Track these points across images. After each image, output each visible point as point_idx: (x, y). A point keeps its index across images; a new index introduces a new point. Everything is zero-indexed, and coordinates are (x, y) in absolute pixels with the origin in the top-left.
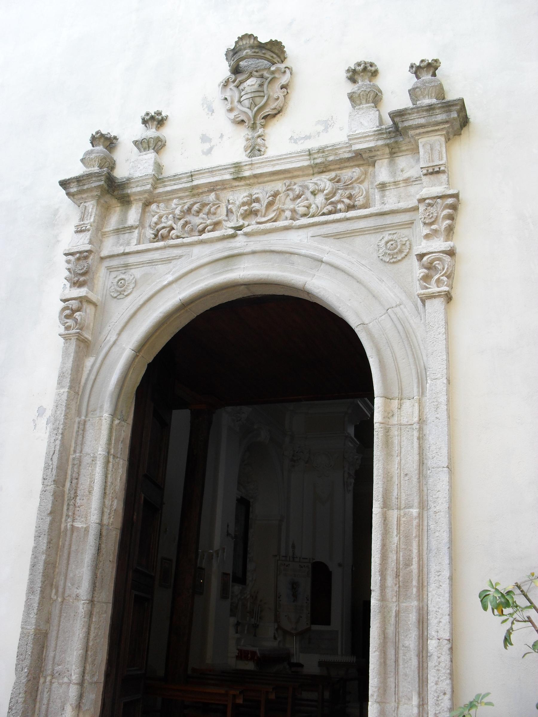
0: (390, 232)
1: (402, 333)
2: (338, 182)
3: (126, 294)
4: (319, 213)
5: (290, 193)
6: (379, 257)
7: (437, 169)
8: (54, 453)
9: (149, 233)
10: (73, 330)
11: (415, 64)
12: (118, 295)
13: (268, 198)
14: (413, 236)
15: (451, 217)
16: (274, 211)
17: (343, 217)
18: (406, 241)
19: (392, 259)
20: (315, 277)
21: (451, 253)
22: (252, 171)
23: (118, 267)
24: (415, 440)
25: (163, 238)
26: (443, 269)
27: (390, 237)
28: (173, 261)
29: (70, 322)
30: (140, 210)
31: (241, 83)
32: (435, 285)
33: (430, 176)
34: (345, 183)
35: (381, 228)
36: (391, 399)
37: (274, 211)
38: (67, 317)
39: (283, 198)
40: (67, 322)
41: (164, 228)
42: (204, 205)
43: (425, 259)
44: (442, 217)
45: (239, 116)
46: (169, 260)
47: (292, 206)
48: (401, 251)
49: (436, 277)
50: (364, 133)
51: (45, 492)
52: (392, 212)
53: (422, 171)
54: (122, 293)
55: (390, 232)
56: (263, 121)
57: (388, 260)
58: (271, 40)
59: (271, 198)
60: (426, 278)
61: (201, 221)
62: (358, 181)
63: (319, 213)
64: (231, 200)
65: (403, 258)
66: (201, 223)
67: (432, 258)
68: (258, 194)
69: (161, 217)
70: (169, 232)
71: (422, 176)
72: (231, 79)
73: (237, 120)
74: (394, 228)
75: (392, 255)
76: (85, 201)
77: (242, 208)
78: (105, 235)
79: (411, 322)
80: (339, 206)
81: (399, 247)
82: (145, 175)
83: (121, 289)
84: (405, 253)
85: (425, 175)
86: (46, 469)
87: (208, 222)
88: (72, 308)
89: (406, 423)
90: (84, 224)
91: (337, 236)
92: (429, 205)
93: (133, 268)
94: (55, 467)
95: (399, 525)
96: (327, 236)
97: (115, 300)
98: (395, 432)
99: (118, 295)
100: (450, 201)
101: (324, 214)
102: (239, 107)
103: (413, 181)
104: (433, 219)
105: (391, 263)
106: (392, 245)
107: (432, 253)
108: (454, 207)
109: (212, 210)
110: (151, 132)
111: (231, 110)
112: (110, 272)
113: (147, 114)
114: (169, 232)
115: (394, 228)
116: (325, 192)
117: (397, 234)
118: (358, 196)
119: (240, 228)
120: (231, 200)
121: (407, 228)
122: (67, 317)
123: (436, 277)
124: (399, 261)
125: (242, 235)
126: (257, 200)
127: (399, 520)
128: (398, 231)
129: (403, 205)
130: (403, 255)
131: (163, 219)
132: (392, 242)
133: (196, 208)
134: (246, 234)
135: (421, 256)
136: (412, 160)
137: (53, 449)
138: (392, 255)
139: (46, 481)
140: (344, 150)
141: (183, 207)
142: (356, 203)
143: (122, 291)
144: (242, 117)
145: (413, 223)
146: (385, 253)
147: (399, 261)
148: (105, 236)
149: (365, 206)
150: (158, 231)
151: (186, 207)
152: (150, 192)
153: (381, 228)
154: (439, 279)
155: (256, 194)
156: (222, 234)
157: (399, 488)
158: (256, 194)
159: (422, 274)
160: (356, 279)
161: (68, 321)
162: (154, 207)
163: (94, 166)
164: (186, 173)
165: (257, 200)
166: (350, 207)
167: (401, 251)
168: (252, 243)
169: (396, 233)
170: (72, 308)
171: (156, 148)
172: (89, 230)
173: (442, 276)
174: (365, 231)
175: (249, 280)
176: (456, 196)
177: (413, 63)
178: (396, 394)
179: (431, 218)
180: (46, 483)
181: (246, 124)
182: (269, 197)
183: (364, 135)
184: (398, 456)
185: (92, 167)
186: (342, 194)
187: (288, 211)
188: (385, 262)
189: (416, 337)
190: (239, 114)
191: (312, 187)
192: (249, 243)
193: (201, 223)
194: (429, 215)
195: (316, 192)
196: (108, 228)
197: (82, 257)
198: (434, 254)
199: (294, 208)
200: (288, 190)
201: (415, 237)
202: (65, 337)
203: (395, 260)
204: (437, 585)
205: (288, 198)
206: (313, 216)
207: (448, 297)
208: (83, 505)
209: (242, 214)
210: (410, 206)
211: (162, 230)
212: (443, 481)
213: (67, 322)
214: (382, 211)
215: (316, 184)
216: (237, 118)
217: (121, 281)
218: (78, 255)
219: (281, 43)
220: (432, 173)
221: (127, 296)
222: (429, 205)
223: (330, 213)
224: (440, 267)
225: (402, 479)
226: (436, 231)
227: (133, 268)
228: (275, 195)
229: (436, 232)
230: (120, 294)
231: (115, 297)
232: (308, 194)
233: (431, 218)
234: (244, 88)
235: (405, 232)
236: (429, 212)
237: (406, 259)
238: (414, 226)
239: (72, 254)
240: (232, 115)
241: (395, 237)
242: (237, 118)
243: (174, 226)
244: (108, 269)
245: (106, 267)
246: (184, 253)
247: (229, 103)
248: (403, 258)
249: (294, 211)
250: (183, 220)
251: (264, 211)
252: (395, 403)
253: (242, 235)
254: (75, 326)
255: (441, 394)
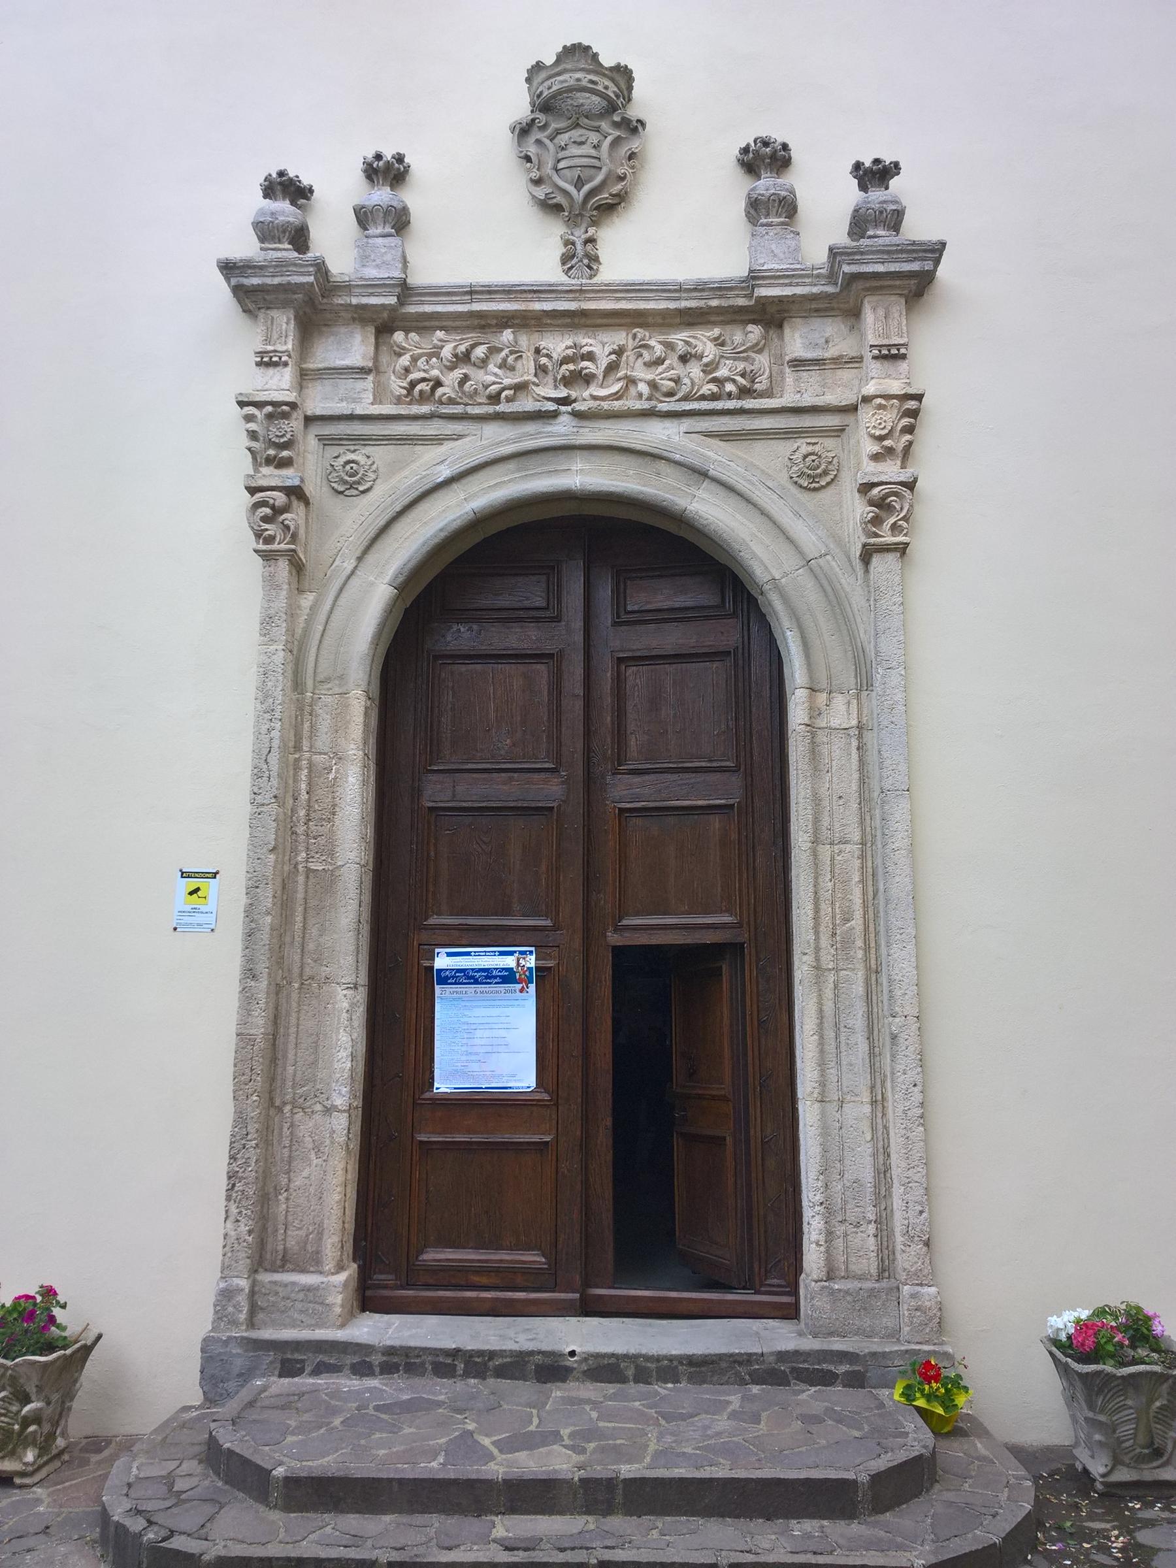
0: (809, 440)
1: (832, 597)
2: (722, 344)
3: (361, 488)
4: (695, 394)
5: (645, 353)
6: (792, 478)
7: (894, 351)
8: (270, 751)
9: (397, 386)
10: (279, 544)
11: (863, 164)
12: (347, 489)
13: (607, 356)
14: (843, 452)
15: (909, 430)
16: (619, 379)
17: (738, 406)
18: (833, 457)
19: (811, 483)
20: (696, 499)
21: (910, 485)
22: (580, 303)
23: (340, 439)
24: (854, 751)
25: (423, 398)
26: (902, 509)
27: (810, 449)
28: (446, 443)
29: (271, 529)
30: (373, 340)
31: (558, 133)
32: (889, 533)
33: (883, 360)
34: (734, 348)
35: (796, 433)
36: (816, 691)
37: (619, 379)
38: (265, 519)
39: (632, 359)
40: (267, 530)
41: (424, 380)
42: (494, 350)
43: (876, 491)
44: (899, 429)
45: (553, 195)
46: (438, 440)
47: (650, 377)
48: (825, 473)
49: (892, 520)
50: (778, 270)
51: (259, 814)
52: (814, 410)
53: (871, 351)
54: (355, 486)
55: (809, 440)
56: (595, 213)
57: (806, 485)
58: (619, 64)
59: (613, 357)
60: (877, 521)
61: (493, 379)
62: (756, 349)
63: (695, 394)
64: (544, 348)
65: (828, 484)
66: (494, 383)
67: (887, 491)
68: (591, 345)
69: (415, 359)
70: (433, 389)
71: (868, 356)
72: (539, 122)
73: (550, 202)
74: (813, 435)
75: (813, 478)
76: (268, 306)
77: (564, 367)
78: (306, 375)
79: (843, 581)
80: (729, 387)
81: (823, 467)
82: (389, 278)
83: (352, 479)
84: (832, 477)
85: (875, 358)
86: (256, 777)
87: (507, 381)
88: (274, 504)
89: (838, 727)
90: (275, 351)
91: (726, 436)
92: (880, 407)
93: (370, 445)
94: (274, 774)
95: (833, 865)
96: (709, 435)
97: (341, 497)
98: (822, 737)
99: (347, 489)
100: (912, 404)
101: (703, 398)
102: (556, 178)
103: (845, 362)
104: (886, 431)
105: (810, 489)
106: (813, 461)
107: (887, 483)
108: (914, 414)
109: (510, 360)
110: (382, 195)
111: (537, 182)
112: (325, 445)
113: (379, 157)
114: (433, 389)
115: (813, 435)
116: (705, 360)
117: (819, 445)
118: (757, 375)
119: (565, 401)
120: (544, 348)
121: (832, 436)
122: (265, 519)
123: (892, 520)
124: (823, 487)
125: (569, 413)
126: (590, 357)
127: (832, 859)
128: (821, 440)
129: (830, 399)
130: (828, 479)
131: (421, 363)
132: (814, 457)
133: (480, 351)
134: (577, 415)
135: (866, 488)
136: (843, 326)
137: (267, 745)
138: (813, 477)
139: (259, 797)
140: (737, 292)
141: (456, 347)
142: (756, 386)
143: (355, 483)
144: (559, 199)
145: (844, 430)
146: (803, 474)
147: (823, 487)
148: (306, 378)
149: (768, 394)
150: (413, 384)
151: (462, 348)
152: (392, 309)
153: (796, 433)
154: (894, 525)
155: (586, 345)
156: (537, 409)
157: (831, 816)
158: (586, 345)
159: (871, 515)
160: (759, 509)
161: (267, 526)
162: (399, 336)
163: (279, 240)
164: (462, 287)
165: (590, 357)
166: (745, 392)
167: (825, 473)
168: (587, 430)
169: (817, 443)
170: (274, 504)
171: (397, 226)
172: (286, 364)
173: (899, 520)
174: (768, 434)
175: (642, 496)
176: (919, 397)
177: (861, 161)
178: (824, 684)
179: (882, 429)
180: (259, 799)
181: (566, 214)
182: (610, 354)
183: (778, 273)
184: (828, 772)
185: (277, 241)
186: (731, 367)
187: (643, 383)
188: (801, 486)
189: (850, 605)
190: (552, 193)
191: (681, 348)
192: (581, 430)
193: (494, 383)
194: (880, 424)
195: (689, 356)
196: (309, 362)
197: (279, 413)
198: (889, 486)
199: (654, 380)
200: (640, 347)
201: (846, 452)
202: (266, 556)
203: (817, 485)
204: (900, 946)
205: (640, 360)
206: (685, 398)
207: (902, 550)
208: (323, 835)
209: (564, 377)
210: (843, 404)
211: (422, 384)
212: (903, 808)
213: (267, 530)
214: (800, 405)
215: (687, 342)
216: (549, 199)
217: (352, 465)
218: (269, 409)
219: (631, 71)
220: (885, 357)
221: (363, 492)
222: (880, 407)
223: (714, 397)
224: (898, 507)
225: (834, 803)
226: (890, 451)
227: (370, 445)
228: (619, 352)
229: (890, 451)
230: (349, 489)
231: (341, 493)
232: (672, 360)
233: (882, 429)
234: (566, 145)
235: (829, 443)
236: (881, 418)
237: (833, 486)
238: (844, 436)
239: (259, 405)
240: (540, 192)
241: (817, 448)
242: (549, 199)
243: (443, 379)
244: (319, 440)
245: (316, 436)
246: (467, 433)
247: (534, 167)
248: (828, 484)
249: (653, 385)
250: (460, 372)
251: (601, 377)
252: (822, 698)
253: (569, 413)
254: (282, 537)
255: (897, 690)
